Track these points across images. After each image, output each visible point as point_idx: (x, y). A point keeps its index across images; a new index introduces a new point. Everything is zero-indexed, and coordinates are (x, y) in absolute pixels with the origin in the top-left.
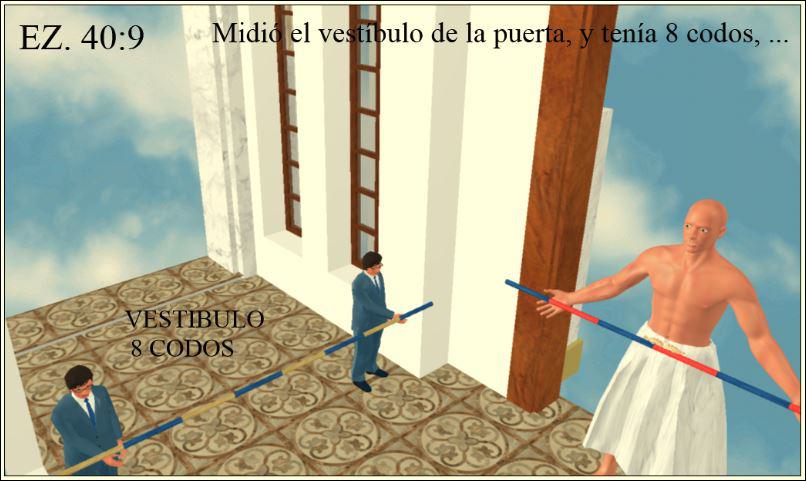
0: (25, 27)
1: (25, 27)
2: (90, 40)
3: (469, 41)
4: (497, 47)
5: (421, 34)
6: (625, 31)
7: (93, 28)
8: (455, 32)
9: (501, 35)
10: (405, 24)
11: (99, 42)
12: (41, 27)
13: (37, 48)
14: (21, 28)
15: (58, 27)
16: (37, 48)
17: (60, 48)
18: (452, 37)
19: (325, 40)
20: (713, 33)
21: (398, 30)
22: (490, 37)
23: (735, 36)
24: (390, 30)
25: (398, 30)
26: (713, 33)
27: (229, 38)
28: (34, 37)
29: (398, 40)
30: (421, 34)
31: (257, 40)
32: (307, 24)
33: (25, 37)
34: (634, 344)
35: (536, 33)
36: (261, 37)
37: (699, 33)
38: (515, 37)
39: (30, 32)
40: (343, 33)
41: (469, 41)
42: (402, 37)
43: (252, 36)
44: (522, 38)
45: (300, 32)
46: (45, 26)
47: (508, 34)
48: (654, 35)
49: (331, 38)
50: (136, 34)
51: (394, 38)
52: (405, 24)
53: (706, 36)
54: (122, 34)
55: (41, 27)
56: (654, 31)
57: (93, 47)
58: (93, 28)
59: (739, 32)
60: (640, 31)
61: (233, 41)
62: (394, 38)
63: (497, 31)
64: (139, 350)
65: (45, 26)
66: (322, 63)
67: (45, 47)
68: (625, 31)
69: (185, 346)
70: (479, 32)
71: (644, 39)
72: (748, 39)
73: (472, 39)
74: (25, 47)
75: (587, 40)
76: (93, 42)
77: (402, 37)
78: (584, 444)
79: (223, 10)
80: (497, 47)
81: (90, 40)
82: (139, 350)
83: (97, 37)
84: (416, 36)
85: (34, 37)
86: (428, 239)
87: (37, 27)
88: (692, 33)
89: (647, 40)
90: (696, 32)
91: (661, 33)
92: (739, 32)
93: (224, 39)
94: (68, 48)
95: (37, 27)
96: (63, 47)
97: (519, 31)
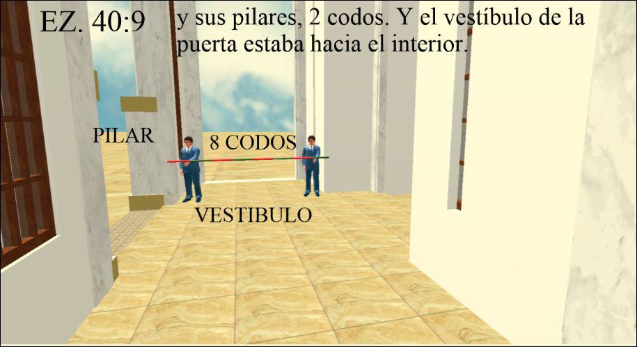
0: (44, 13)
2: (100, 24)
3: (571, 23)
4: (235, 29)
7: (102, 13)
8: (559, 16)
9: (238, 19)
10: (517, 9)
12: (58, 13)
13: (55, 30)
14: (42, 13)
15: (73, 13)
16: (55, 30)
18: (556, 20)
19: (449, 23)
21: (511, 15)
23: (368, 19)
24: (504, 15)
25: (511, 15)
28: (53, 21)
29: (511, 23)
32: (434, 9)
33: (45, 21)
37: (240, 138)
40: (464, 16)
41: (571, 23)
42: (514, 21)
45: (428, 16)
46: (62, 12)
49: (454, 21)
50: (138, 18)
51: (507, 21)
52: (517, 9)
53: (344, 19)
54: (127, 18)
55: (58, 13)
57: (102, 30)
58: (102, 13)
60: (347, 42)
62: (507, 21)
63: (235, 15)
64: (217, 144)
67: (61, 30)
70: (579, 16)
71: (257, 22)
72: (379, 22)
73: (574, 22)
75: (183, 22)
76: (102, 25)
77: (514, 21)
80: (235, 29)
81: (100, 24)
82: (217, 144)
83: (106, 22)
84: (526, 19)
85: (53, 21)
87: (55, 12)
88: (332, 16)
90: (336, 16)
94: (80, 31)
96: (77, 30)
97: (198, 42)
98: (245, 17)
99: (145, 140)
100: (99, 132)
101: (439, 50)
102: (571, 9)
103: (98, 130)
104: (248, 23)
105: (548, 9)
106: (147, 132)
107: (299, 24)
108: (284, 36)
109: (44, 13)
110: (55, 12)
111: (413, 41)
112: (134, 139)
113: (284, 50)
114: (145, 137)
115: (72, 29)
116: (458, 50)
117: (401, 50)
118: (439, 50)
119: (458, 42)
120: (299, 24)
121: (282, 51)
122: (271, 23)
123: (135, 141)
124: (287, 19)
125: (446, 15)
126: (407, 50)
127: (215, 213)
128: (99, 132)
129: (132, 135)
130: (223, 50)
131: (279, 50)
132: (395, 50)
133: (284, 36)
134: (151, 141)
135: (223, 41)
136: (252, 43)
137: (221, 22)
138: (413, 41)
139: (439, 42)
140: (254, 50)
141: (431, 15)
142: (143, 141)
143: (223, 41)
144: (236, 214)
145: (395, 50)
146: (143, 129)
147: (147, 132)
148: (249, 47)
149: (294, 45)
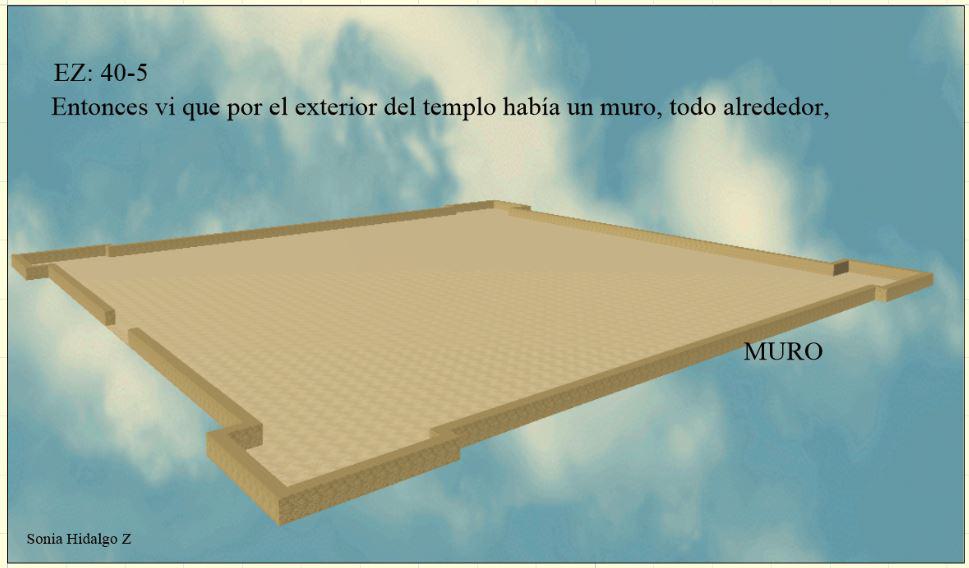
0: (55, 99)
1: (58, 65)
5: (713, 106)
7: (109, 66)
9: (234, 109)
12: (70, 65)
15: (83, 65)
18: (214, 110)
19: (161, 112)
20: (240, 107)
26: (240, 107)
27: (759, 356)
30: (713, 106)
31: (465, 105)
33: (58, 72)
35: (442, 107)
36: (462, 108)
37: (788, 106)
38: (108, 108)
42: (735, 110)
45: (406, 106)
55: (70, 65)
56: (557, 105)
58: (109, 66)
59: (358, 113)
60: (545, 105)
61: (763, 358)
67: (73, 80)
69: (815, 108)
71: (516, 112)
74: (58, 79)
76: (109, 76)
80: (230, 119)
84: (490, 109)
90: (124, 106)
91: (121, 539)
92: (358, 113)
93: (755, 357)
97: (205, 105)
98: (542, 108)
101: (352, 114)
104: (104, 113)
105: (798, 99)
107: (659, 114)
108: (531, 99)
111: (84, 103)
116: (817, 114)
117: (739, 114)
118: (352, 114)
119: (257, 105)
120: (659, 114)
121: (367, 105)
122: (637, 114)
124: (138, 109)
125: (172, 113)
127: (58, 104)
131: (525, 113)
132: (506, 113)
133: (531, 99)
136: (135, 106)
137: (143, 112)
138: (84, 103)
139: (351, 105)
140: (138, 113)
141: (410, 105)
143: (323, 103)
145: (506, 113)
148: (301, 110)
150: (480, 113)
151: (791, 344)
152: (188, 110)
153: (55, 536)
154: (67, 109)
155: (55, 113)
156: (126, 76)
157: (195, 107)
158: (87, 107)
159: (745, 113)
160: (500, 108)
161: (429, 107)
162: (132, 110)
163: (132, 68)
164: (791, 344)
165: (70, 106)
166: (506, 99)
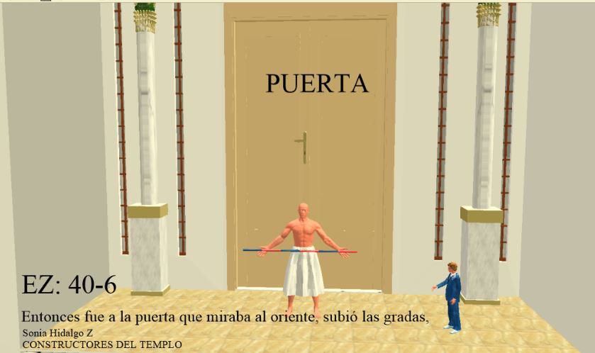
0: (26, 277)
1: (26, 277)
4: (137, 324)
6: (297, 316)
7: (77, 277)
11: (82, 288)
12: (38, 277)
13: (35, 292)
15: (51, 277)
17: (52, 292)
22: (133, 318)
23: (48, 318)
28: (33, 284)
32: (264, 312)
33: (26, 284)
34: (129, 204)
38: (147, 319)
39: (30, 280)
41: (364, 321)
43: (63, 334)
44: (97, 319)
46: (41, 276)
47: (144, 318)
48: (249, 318)
55: (38, 277)
57: (77, 292)
58: (77, 277)
65: (41, 276)
66: (17, 300)
67: (40, 292)
68: (297, 316)
74: (26, 292)
76: (77, 288)
77: (39, 319)
78: (314, 256)
79: (318, 255)
80: (270, 91)
83: (80, 285)
84: (274, 318)
85: (33, 284)
86: (8, 93)
89: (389, 316)
94: (58, 293)
95: (35, 276)
99: (322, 90)
100: (274, 80)
102: (364, 312)
103: (323, 77)
104: (53, 321)
106: (324, 79)
108: (339, 312)
109: (24, 312)
110: (35, 276)
111: (41, 315)
112: (362, 88)
113: (339, 320)
114: (323, 86)
115: (50, 291)
117: (221, 321)
121: (98, 321)
123: (363, 90)
124: (74, 318)
126: (37, 321)
128: (274, 80)
129: (359, 83)
130: (166, 320)
132: (208, 320)
134: (330, 91)
135: (166, 315)
139: (286, 316)
142: (320, 91)
143: (166, 315)
144: (52, 344)
145: (208, 320)
146: (270, 76)
147: (324, 79)
149: (244, 318)
150: (348, 321)
151: (320, 76)
152: (183, 318)
153: (168, 314)
154: (31, 317)
155: (24, 321)
156: (104, 285)
157: (303, 320)
158: (43, 317)
159: (225, 321)
160: (118, 318)
161: (346, 319)
162: (70, 319)
163: (100, 281)
164: (320, 76)
165: (33, 316)
166: (365, 91)
